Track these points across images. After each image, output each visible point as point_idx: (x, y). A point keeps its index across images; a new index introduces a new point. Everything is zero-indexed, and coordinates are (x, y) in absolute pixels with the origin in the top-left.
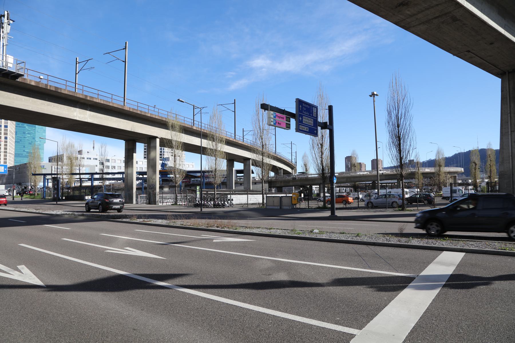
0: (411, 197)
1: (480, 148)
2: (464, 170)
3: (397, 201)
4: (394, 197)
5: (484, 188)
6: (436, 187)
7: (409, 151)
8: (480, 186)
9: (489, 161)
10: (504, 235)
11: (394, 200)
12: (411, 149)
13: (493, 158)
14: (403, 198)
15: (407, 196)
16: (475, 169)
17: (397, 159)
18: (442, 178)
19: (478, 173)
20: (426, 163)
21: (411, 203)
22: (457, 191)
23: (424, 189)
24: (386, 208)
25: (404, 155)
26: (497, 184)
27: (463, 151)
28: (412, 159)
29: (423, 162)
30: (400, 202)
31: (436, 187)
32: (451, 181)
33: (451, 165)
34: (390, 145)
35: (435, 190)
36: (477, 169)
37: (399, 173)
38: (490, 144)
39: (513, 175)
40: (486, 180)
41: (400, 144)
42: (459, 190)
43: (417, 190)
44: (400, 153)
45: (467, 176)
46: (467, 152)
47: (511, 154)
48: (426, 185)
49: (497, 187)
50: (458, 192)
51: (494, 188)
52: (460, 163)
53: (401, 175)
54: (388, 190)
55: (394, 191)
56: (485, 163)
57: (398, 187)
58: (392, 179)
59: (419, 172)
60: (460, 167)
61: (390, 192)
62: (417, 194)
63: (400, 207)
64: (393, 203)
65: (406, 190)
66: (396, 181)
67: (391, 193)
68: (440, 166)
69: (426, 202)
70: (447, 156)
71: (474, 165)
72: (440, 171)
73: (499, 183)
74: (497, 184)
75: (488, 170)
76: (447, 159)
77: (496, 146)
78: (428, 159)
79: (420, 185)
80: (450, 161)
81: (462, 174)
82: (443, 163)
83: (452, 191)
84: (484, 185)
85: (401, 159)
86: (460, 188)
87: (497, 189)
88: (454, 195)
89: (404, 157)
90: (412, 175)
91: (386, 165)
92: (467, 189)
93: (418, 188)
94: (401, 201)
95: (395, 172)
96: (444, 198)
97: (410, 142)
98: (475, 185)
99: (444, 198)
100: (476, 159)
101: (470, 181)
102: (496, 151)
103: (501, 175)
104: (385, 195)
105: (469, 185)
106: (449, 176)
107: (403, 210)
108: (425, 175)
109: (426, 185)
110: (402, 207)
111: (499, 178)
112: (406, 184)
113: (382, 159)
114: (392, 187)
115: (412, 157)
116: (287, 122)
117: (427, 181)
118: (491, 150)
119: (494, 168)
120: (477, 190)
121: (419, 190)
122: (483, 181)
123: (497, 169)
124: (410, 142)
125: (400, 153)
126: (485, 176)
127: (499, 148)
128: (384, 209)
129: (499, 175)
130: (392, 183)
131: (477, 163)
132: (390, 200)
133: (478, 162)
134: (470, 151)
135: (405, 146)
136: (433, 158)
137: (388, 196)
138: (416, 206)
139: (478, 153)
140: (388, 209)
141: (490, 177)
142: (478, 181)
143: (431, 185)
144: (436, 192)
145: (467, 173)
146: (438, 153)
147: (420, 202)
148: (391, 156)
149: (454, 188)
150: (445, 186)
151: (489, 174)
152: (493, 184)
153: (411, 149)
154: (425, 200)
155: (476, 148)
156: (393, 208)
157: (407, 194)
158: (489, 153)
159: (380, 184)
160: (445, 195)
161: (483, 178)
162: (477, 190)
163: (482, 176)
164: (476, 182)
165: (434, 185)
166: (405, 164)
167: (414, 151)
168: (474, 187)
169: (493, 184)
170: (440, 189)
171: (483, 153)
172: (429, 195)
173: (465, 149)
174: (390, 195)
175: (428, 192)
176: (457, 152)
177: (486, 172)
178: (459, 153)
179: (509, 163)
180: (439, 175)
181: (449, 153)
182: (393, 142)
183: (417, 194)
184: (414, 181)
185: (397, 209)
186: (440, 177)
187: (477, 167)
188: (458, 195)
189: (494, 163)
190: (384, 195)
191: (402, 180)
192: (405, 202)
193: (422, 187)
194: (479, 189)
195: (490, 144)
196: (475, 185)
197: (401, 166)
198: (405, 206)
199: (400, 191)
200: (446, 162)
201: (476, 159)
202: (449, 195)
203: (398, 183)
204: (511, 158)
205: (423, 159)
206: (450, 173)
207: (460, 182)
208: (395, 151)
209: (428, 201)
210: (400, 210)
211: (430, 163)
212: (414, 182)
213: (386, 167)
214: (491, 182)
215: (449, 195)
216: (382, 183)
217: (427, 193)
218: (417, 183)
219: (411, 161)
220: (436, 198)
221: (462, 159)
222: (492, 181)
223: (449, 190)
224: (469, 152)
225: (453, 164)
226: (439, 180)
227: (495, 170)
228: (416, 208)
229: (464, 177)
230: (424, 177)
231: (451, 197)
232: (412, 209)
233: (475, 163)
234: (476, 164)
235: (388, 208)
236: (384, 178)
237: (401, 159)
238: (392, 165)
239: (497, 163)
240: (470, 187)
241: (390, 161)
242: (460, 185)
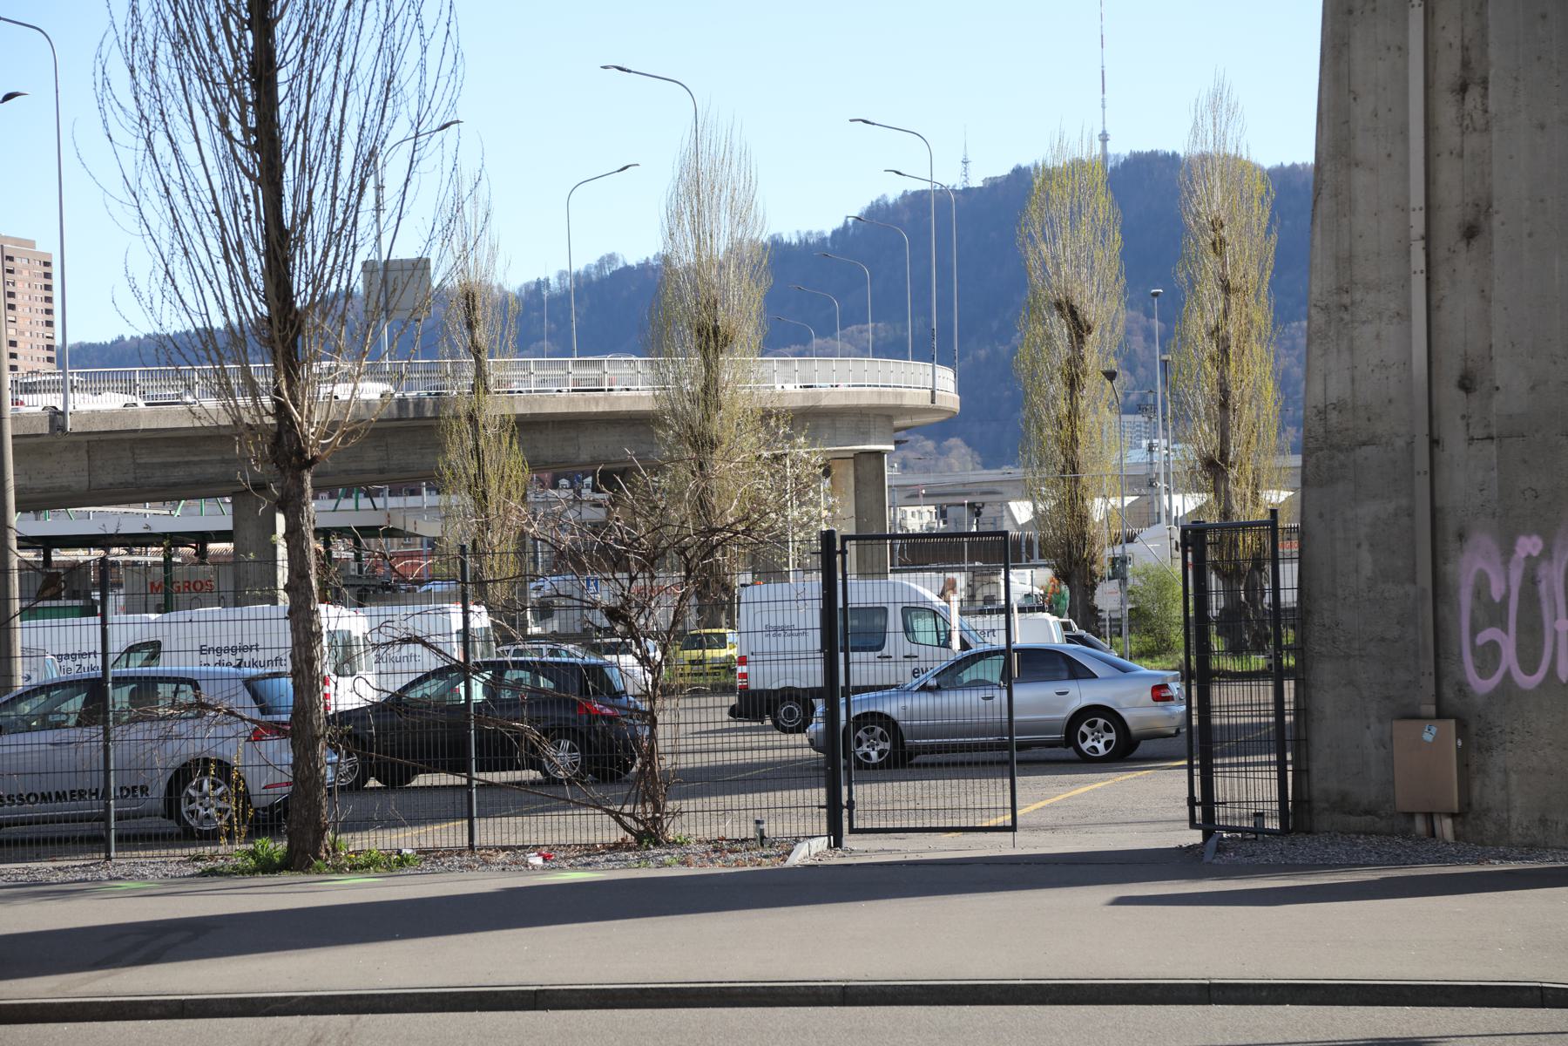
0: (394, 706)
1: (1122, 147)
2: (962, 389)
3: (235, 750)
4: (201, 707)
5: (1162, 586)
6: (670, 579)
7: (369, 161)
8: (1119, 567)
9: (1209, 288)
10: (60, 556)
11: (198, 740)
12: (401, 129)
13: (1250, 256)
14: (301, 725)
15: (348, 693)
16: (1073, 383)
17: (232, 252)
18: (735, 481)
19: (1101, 418)
20: (561, 300)
21: (396, 779)
22: (894, 622)
23: (544, 611)
24: (97, 842)
25: (313, 195)
26: (1289, 547)
27: (951, 178)
28: (406, 250)
29: (535, 292)
30: (267, 767)
31: (670, 579)
32: (831, 509)
33: (827, 331)
34: (141, 65)
35: (662, 616)
36: (1092, 382)
37: (256, 409)
38: (1218, 103)
39: (1434, 442)
40: (1184, 504)
41: (263, 69)
42: (910, 612)
43: (450, 622)
44: (270, 179)
45: (991, 459)
46: (994, 186)
47: (1417, 222)
48: (566, 560)
49: (1289, 574)
50: (895, 642)
51: (1254, 590)
52: (923, 310)
53: (284, 445)
54: (128, 628)
55: (195, 639)
56: (1173, 308)
57: (246, 584)
58: (167, 493)
59: (495, 408)
60: (922, 355)
61: (153, 649)
62: (463, 670)
63: (263, 822)
64: (182, 776)
65: (336, 619)
66: (214, 515)
67: (165, 666)
68: (712, 339)
69: (562, 757)
70: (790, 235)
71: (1059, 328)
72: (709, 393)
73: (1303, 534)
74: (1289, 547)
75: (1202, 396)
76: (784, 261)
77: (1280, 128)
78: (584, 259)
79: (500, 565)
80: (817, 288)
81: (943, 428)
82: (742, 308)
83: (842, 630)
84: (1156, 552)
85: (280, 244)
86: (923, 586)
87: (1289, 598)
88: (862, 668)
89: (319, 225)
90: (403, 447)
91: (94, 319)
92: (988, 607)
93: (471, 588)
94: (280, 751)
95: (209, 407)
96: (756, 706)
97: (389, 53)
98: (1074, 565)
99: (756, 706)
100: (1083, 264)
101: (1022, 511)
102: (1282, 178)
103: (1326, 455)
104: (94, 689)
105: (1002, 551)
106: (806, 451)
107: (299, 860)
108: (558, 445)
109: (566, 560)
110: (291, 830)
111: (1308, 482)
112: (342, 550)
113: (47, 245)
114: (166, 593)
115: (407, 226)
116: (1125, 624)
117: (573, 510)
118: (1235, 169)
119: (1257, 373)
120: (1087, 614)
121: (481, 620)
122: (1148, 515)
123: (1283, 382)
124: (389, 53)
125: (270, 179)
126: (1171, 452)
127: (1310, 159)
128: (71, 866)
129: (1307, 450)
130: (175, 539)
131: (1092, 311)
132: (147, 749)
133: (1104, 308)
134: (1019, 174)
135: (327, 98)
136: (639, 244)
137: (119, 698)
138: (461, 807)
139: (1103, 203)
140: (123, 860)
141: (1215, 468)
142: (1098, 508)
143: (619, 562)
144: (675, 635)
145: (995, 418)
146: (696, 192)
147: (499, 753)
148: (155, 209)
149: (860, 592)
150: (770, 572)
151: (1205, 436)
152: (1248, 541)
153: (401, 129)
154: (554, 733)
155: (1081, 147)
156: (189, 836)
157: (346, 665)
158: (1213, 200)
159: (18, 556)
160: (762, 677)
161: (1146, 483)
162: (1087, 614)
163: (1137, 456)
164: (1083, 519)
165: (651, 561)
166: (325, 305)
167: (433, 153)
168: (1063, 575)
169: (1248, 541)
170: (715, 600)
171: (1149, 198)
172: (597, 672)
173: (970, 151)
174: (145, 687)
175: (584, 638)
176: (893, 190)
177: (1181, 417)
178: (916, 202)
179: (1404, 316)
180: (703, 443)
181: (809, 195)
182: (182, 40)
183: (463, 670)
184: (427, 515)
185: (232, 851)
186: (719, 465)
187: (1094, 357)
188: (901, 673)
189: (1261, 315)
190: (70, 686)
191: (292, 504)
192: (331, 765)
193: (523, 578)
194: (1108, 598)
195: (1218, 103)
196: (1074, 565)
197: (286, 329)
198: (328, 812)
199: (264, 630)
200: (774, 302)
201: (1083, 264)
202: (811, 674)
203: (250, 532)
204: (1418, 261)
205: (529, 251)
206: (812, 419)
207: (918, 519)
208: (204, 153)
209: (581, 739)
210: (267, 867)
211: (614, 307)
212: (429, 528)
213: (103, 334)
214: (1230, 528)
215: (811, 674)
216: (46, 544)
217: (573, 654)
218: (456, 533)
219: (396, 281)
220: (667, 711)
221: (937, 265)
222: (1241, 513)
223: (811, 617)
224: (1016, 190)
225: (853, 317)
226: (702, 504)
227: (1270, 391)
228: (449, 834)
229: (961, 466)
230: (535, 464)
231: (831, 690)
232: (406, 839)
233: (1069, 311)
234: (1080, 329)
235: (130, 840)
236: (70, 473)
237: (280, 244)
238: (176, 323)
239: (1281, 316)
240: (1026, 581)
241: (144, 265)
242: (922, 552)
